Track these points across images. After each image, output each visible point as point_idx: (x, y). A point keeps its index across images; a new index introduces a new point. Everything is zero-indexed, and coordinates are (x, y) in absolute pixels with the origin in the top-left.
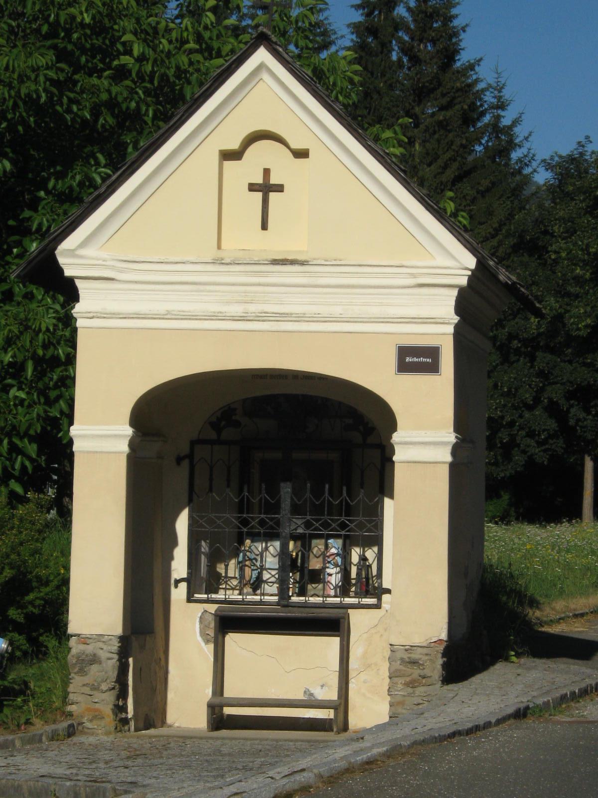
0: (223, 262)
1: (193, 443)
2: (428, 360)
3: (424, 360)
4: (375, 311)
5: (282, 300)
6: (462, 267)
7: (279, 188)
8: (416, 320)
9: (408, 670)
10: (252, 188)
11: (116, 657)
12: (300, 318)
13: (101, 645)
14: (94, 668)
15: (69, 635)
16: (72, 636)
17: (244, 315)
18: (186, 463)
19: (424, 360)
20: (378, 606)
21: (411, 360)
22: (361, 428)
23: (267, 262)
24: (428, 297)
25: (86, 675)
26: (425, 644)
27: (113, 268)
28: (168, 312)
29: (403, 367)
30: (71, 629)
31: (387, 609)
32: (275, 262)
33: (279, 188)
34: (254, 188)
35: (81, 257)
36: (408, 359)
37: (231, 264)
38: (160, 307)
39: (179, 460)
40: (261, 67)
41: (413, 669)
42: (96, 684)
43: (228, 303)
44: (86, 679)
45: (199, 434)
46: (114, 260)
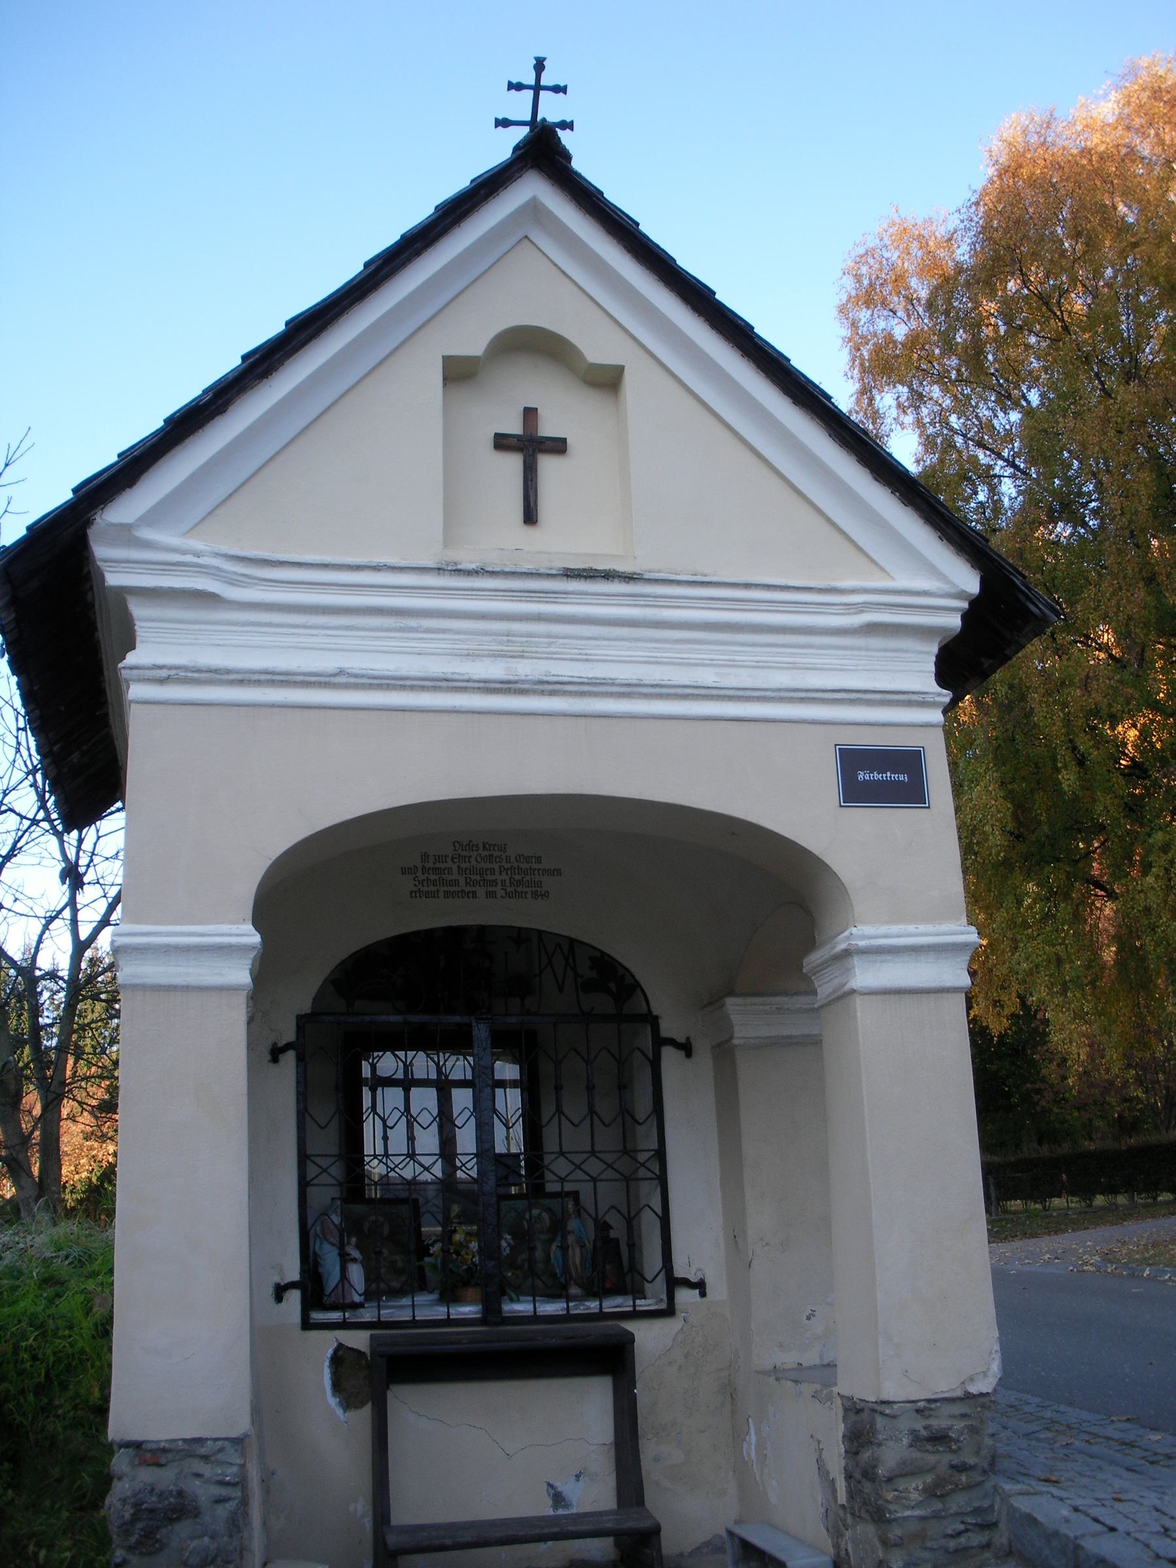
0: (459, 567)
3: (895, 777)
6: (953, 591)
7: (558, 446)
8: (869, 696)
10: (502, 443)
12: (630, 690)
14: (184, 1528)
15: (111, 1444)
18: (290, 1058)
19: (895, 777)
22: (612, 985)
24: (883, 654)
25: (161, 1549)
28: (341, 672)
32: (570, 574)
33: (558, 446)
34: (504, 442)
36: (861, 776)
38: (327, 663)
41: (938, 1451)
43: (469, 655)
46: (217, 555)
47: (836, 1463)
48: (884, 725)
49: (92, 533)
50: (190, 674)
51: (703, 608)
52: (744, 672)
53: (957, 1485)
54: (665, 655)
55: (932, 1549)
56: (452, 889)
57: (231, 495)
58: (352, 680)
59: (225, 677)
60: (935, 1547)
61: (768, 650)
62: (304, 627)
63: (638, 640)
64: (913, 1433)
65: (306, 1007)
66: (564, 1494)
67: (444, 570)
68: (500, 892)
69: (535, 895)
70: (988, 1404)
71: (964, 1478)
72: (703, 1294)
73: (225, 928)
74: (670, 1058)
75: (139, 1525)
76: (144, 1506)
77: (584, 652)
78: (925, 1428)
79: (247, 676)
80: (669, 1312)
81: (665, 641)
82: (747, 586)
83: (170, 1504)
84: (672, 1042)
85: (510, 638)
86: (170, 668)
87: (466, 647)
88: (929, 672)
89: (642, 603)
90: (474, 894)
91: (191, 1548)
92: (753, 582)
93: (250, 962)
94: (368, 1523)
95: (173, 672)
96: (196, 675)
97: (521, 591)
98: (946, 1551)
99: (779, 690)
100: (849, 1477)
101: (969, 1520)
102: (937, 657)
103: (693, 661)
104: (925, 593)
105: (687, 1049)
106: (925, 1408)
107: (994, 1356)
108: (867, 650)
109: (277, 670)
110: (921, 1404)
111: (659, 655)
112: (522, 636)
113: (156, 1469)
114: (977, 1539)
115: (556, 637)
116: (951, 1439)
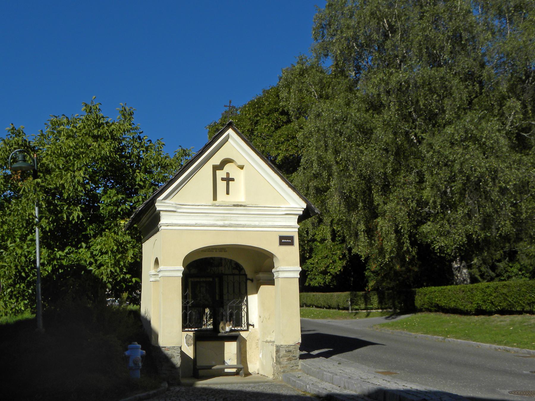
4: (270, 223)
7: (233, 180)
9: (288, 354)
11: (179, 355)
12: (244, 226)
13: (174, 350)
22: (238, 268)
29: (281, 244)
32: (234, 206)
33: (233, 180)
35: (164, 203)
36: (283, 241)
38: (193, 222)
40: (228, 136)
43: (217, 220)
47: (274, 355)
52: (263, 222)
68: (218, 250)
69: (225, 251)
72: (254, 327)
74: (249, 282)
80: (247, 330)
82: (265, 207)
84: (249, 279)
90: (213, 251)
94: (192, 366)
100: (276, 358)
105: (252, 280)
114: (295, 367)
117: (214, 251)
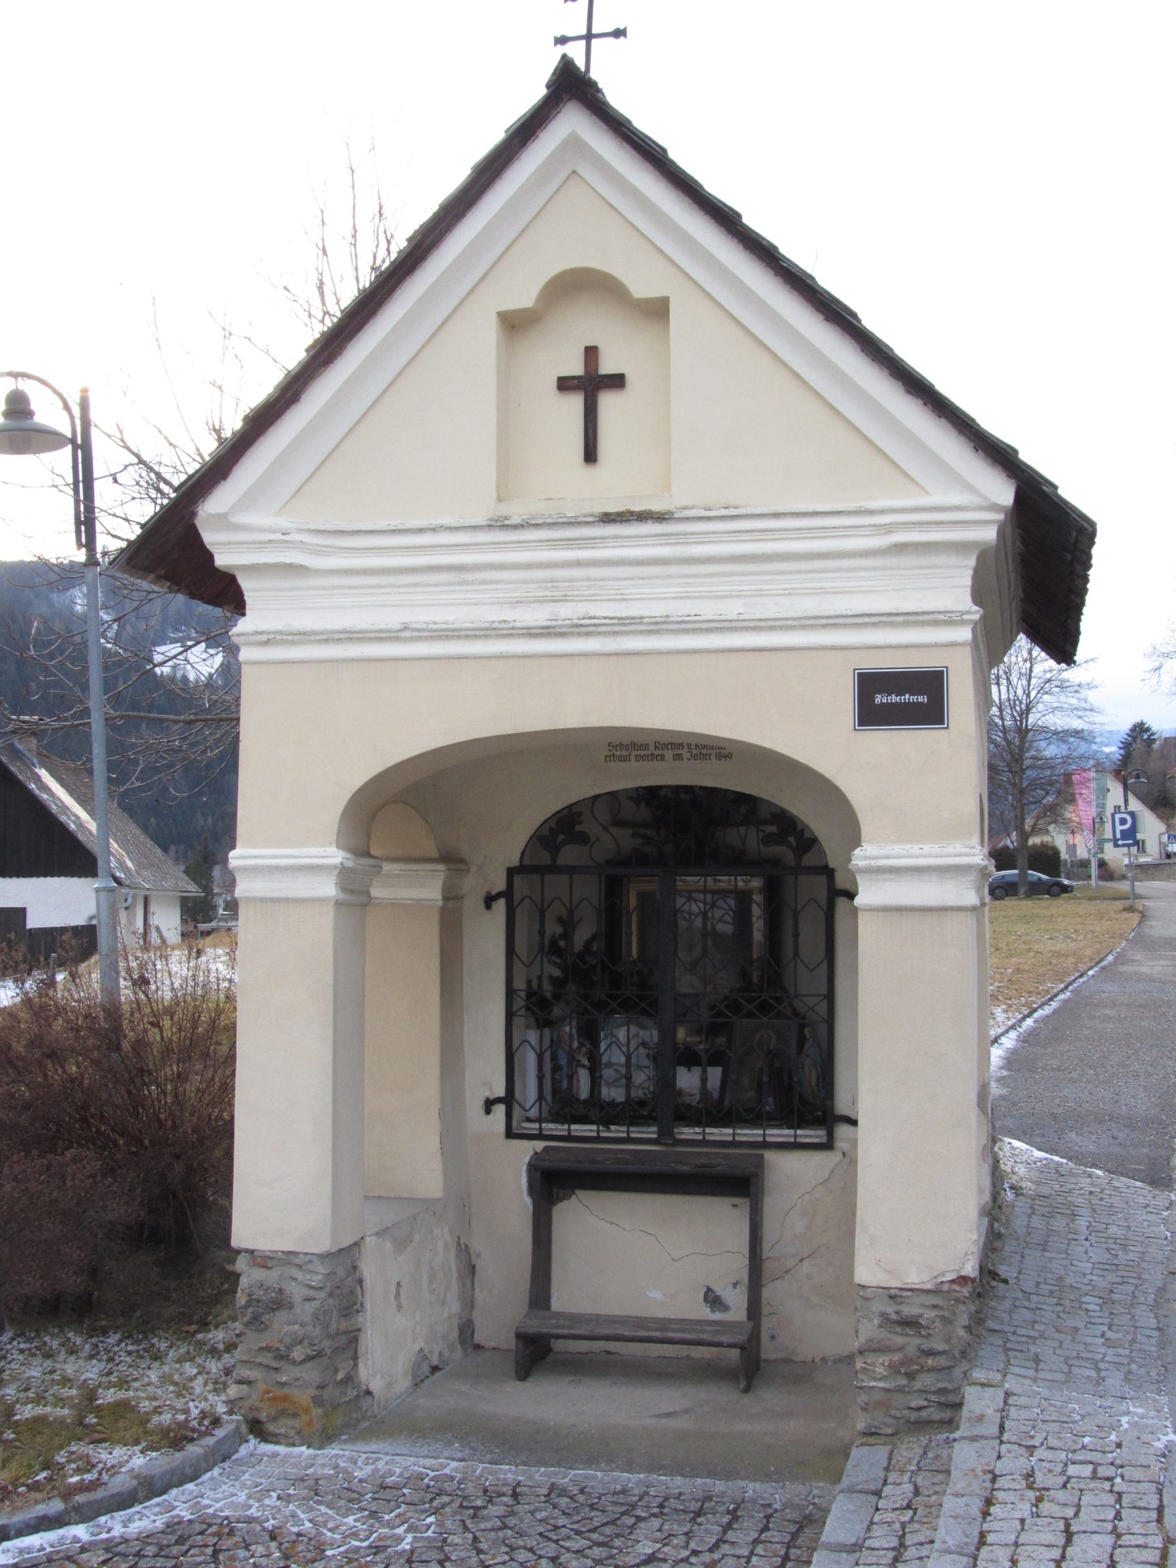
0: (507, 522)
1: (511, 872)
2: (920, 699)
3: (913, 699)
5: (624, 592)
6: (986, 503)
7: (617, 382)
10: (565, 384)
12: (659, 626)
14: (282, 1316)
16: (238, 1252)
17: (549, 623)
18: (500, 906)
19: (913, 699)
20: (828, 1145)
21: (885, 701)
22: (792, 840)
23: (591, 519)
24: (915, 572)
26: (929, 1286)
27: (301, 546)
30: (235, 1242)
31: (845, 1150)
32: (608, 518)
33: (617, 382)
36: (879, 699)
37: (522, 526)
38: (392, 619)
39: (489, 901)
41: (907, 1335)
42: (282, 1348)
44: (265, 1340)
45: (522, 858)
48: (907, 647)
49: (199, 522)
50: (285, 637)
51: (732, 541)
53: (922, 1367)
54: (695, 589)
55: (895, 1417)
56: (642, 753)
57: (314, 473)
58: (416, 634)
59: (312, 638)
60: (899, 1416)
61: (798, 576)
62: (379, 586)
63: (669, 577)
64: (884, 1315)
65: (515, 861)
66: (722, 1298)
67: (494, 526)
68: (686, 755)
70: (962, 1299)
71: (930, 1362)
73: (313, 851)
75: (250, 1310)
76: (254, 1297)
77: (620, 592)
78: (896, 1313)
79: (330, 636)
81: (696, 576)
82: (776, 515)
83: (272, 1297)
85: (554, 584)
86: (269, 633)
87: (515, 595)
88: (966, 587)
89: (674, 541)
90: (663, 757)
91: (285, 1330)
92: (781, 511)
93: (334, 878)
95: (271, 637)
96: (290, 638)
97: (562, 540)
98: (908, 1421)
99: (799, 618)
101: (933, 1398)
102: (976, 570)
103: (721, 593)
104: (958, 508)
106: (894, 1296)
107: (970, 1257)
108: (898, 569)
109: (354, 629)
110: (893, 1292)
111: (689, 589)
112: (564, 581)
113: (262, 1270)
115: (595, 580)
116: (921, 1326)
117: (669, 754)
